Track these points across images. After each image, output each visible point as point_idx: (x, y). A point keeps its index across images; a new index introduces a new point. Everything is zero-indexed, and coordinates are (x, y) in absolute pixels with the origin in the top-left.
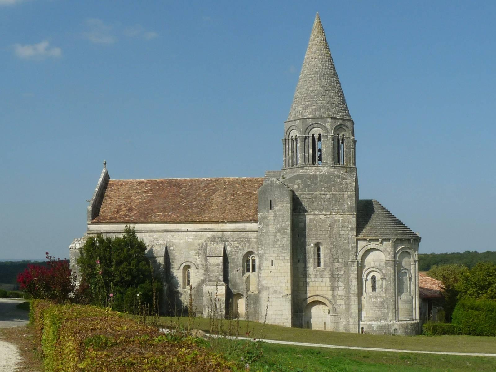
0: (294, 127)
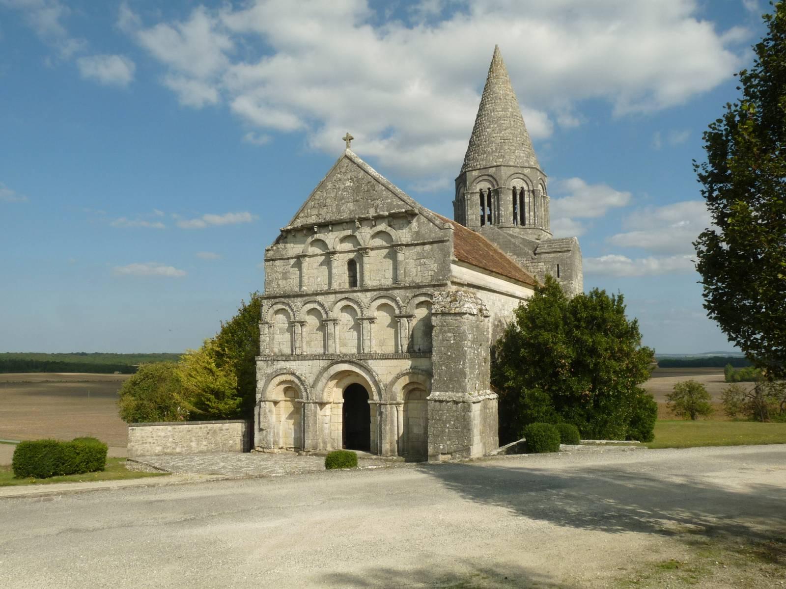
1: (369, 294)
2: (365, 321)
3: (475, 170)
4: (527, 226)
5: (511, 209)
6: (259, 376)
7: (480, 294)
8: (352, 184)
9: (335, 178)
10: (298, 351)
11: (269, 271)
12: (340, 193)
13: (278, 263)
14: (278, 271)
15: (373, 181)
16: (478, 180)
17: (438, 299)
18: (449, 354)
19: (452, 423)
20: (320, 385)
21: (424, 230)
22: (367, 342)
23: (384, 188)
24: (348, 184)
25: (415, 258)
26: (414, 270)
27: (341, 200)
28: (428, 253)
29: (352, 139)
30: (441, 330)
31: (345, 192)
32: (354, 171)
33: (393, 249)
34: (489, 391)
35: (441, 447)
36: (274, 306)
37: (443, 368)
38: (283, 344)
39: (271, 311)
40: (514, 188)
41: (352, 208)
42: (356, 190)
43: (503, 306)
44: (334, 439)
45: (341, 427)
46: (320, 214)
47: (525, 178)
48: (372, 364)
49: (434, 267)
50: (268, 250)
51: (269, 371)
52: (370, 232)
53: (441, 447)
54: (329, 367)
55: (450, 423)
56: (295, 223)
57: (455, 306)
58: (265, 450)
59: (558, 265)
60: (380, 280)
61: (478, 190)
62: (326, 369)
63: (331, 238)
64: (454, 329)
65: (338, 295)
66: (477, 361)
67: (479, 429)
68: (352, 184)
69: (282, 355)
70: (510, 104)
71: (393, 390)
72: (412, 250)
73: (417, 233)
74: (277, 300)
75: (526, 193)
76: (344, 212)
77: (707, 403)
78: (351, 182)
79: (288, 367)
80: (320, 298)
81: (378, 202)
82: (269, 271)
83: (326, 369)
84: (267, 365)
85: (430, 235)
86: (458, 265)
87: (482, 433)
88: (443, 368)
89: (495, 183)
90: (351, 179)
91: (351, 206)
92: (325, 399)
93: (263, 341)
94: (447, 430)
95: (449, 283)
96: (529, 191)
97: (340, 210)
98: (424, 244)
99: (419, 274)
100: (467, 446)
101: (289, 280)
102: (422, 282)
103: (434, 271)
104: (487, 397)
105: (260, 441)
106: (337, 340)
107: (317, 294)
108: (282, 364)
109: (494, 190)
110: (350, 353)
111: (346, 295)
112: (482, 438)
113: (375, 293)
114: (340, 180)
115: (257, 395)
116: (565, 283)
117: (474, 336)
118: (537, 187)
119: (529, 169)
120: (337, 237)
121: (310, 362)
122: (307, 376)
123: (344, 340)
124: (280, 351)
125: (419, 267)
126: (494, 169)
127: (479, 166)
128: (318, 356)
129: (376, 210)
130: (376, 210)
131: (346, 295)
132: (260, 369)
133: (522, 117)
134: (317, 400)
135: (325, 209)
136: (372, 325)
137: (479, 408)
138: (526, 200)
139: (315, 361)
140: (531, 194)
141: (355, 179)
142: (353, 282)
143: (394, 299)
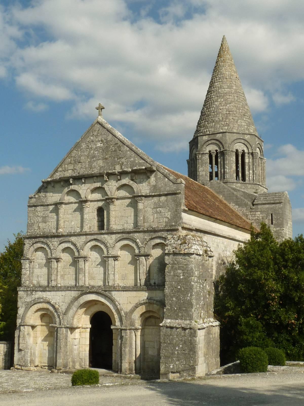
1: (114, 236)
2: (110, 259)
3: (205, 135)
4: (247, 181)
6: (19, 304)
7: (206, 238)
8: (102, 145)
9: (88, 140)
10: (53, 284)
11: (31, 215)
12: (92, 152)
13: (39, 208)
14: (39, 215)
15: (120, 143)
16: (207, 143)
17: (171, 241)
18: (179, 287)
19: (181, 346)
20: (71, 312)
21: (161, 184)
22: (111, 277)
23: (128, 149)
24: (99, 145)
25: (153, 207)
26: (152, 217)
27: (93, 157)
28: (163, 203)
29: (104, 108)
30: (172, 267)
31: (96, 151)
32: (104, 134)
33: (135, 200)
34: (212, 320)
35: (171, 367)
36: (34, 245)
37: (174, 299)
38: (41, 277)
39: (32, 249)
40: (237, 150)
41: (101, 165)
42: (105, 150)
43: (225, 247)
44: (81, 359)
45: (88, 349)
46: (75, 169)
47: (246, 143)
48: (115, 295)
49: (168, 214)
50: (31, 198)
51: (28, 299)
52: (116, 185)
53: (171, 367)
54: (79, 297)
55: (179, 347)
56: (55, 176)
57: (185, 248)
58: (23, 368)
59: (272, 215)
60: (123, 225)
61: (207, 151)
62: (76, 299)
63: (84, 189)
64: (183, 267)
65: (88, 237)
66: (202, 294)
67: (203, 351)
68: (102, 145)
69: (40, 287)
71: (132, 317)
72: (150, 200)
73: (155, 186)
74: (37, 240)
75: (246, 155)
76: (95, 167)
78: (101, 143)
79: (45, 296)
80: (73, 239)
81: (123, 160)
82: (31, 215)
83: (76, 299)
84: (27, 295)
85: (165, 189)
86: (188, 214)
87: (205, 355)
88: (174, 299)
89: (221, 146)
90: (101, 141)
91: (101, 163)
92: (75, 324)
93: (24, 275)
94: (176, 353)
95: (180, 228)
96: (249, 153)
97: (91, 166)
98: (160, 196)
99: (156, 220)
100: (192, 366)
101: (47, 223)
102: (158, 227)
103: (168, 218)
104: (211, 324)
105: (19, 360)
106: (87, 274)
107: (70, 235)
108: (39, 294)
110: (97, 285)
111: (95, 237)
112: (206, 359)
113: (119, 235)
114: (93, 141)
115: (18, 320)
116: (278, 229)
117: (200, 272)
118: (255, 150)
119: (249, 136)
120: (88, 188)
121: (63, 293)
122: (60, 305)
123: (92, 274)
124: (38, 283)
125: (155, 215)
126: (221, 135)
127: (208, 132)
128: (70, 287)
129: (121, 167)
130: (121, 167)
131: (95, 237)
132: (21, 298)
133: (243, 94)
134: (68, 326)
135: (79, 165)
136: (116, 262)
137: (204, 334)
138: (247, 160)
139: (67, 292)
140: (251, 156)
141: (105, 141)
143: (134, 241)
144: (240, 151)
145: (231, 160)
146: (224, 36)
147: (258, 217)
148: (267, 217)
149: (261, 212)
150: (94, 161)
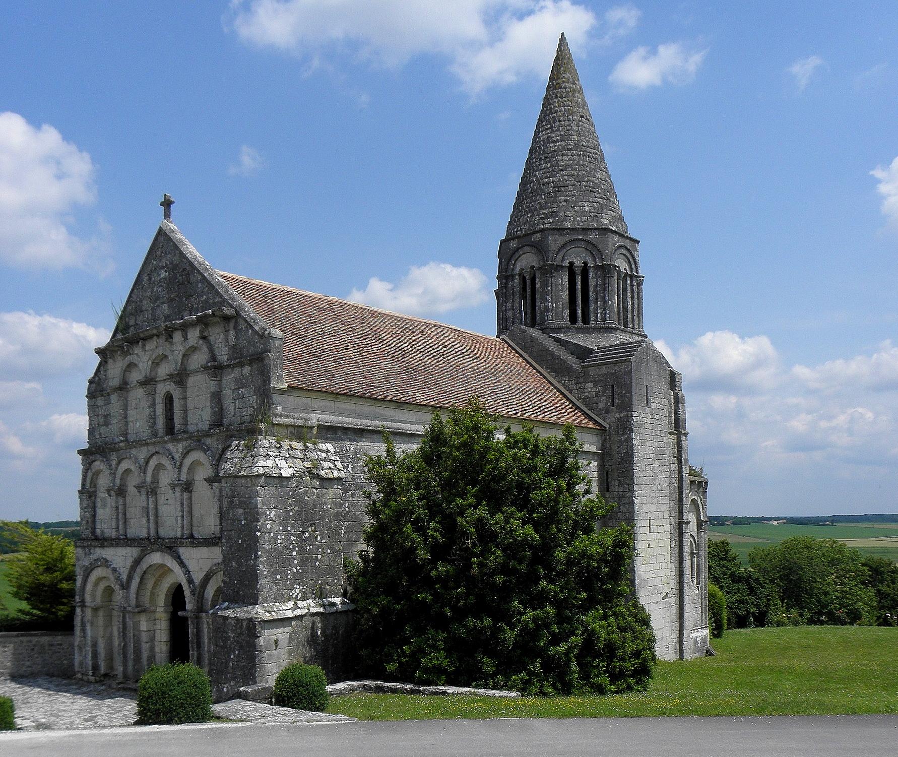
0: (583, 245)
4: (592, 323)
5: (565, 295)
16: (517, 255)
26: (231, 407)
35: (225, 690)
40: (571, 264)
51: (86, 563)
53: (225, 690)
60: (197, 424)
61: (517, 271)
70: (575, 128)
77: (504, 631)
85: (248, 351)
103: (253, 407)
109: (540, 268)
116: (622, 415)
124: (102, 532)
126: (539, 235)
138: (592, 282)
142: (170, 429)
144: (578, 263)
145: (557, 285)
146: (563, 34)
147: (589, 392)
148: (604, 392)
149: (595, 383)
150: (158, 306)
